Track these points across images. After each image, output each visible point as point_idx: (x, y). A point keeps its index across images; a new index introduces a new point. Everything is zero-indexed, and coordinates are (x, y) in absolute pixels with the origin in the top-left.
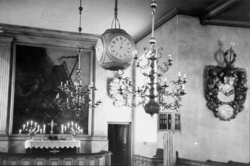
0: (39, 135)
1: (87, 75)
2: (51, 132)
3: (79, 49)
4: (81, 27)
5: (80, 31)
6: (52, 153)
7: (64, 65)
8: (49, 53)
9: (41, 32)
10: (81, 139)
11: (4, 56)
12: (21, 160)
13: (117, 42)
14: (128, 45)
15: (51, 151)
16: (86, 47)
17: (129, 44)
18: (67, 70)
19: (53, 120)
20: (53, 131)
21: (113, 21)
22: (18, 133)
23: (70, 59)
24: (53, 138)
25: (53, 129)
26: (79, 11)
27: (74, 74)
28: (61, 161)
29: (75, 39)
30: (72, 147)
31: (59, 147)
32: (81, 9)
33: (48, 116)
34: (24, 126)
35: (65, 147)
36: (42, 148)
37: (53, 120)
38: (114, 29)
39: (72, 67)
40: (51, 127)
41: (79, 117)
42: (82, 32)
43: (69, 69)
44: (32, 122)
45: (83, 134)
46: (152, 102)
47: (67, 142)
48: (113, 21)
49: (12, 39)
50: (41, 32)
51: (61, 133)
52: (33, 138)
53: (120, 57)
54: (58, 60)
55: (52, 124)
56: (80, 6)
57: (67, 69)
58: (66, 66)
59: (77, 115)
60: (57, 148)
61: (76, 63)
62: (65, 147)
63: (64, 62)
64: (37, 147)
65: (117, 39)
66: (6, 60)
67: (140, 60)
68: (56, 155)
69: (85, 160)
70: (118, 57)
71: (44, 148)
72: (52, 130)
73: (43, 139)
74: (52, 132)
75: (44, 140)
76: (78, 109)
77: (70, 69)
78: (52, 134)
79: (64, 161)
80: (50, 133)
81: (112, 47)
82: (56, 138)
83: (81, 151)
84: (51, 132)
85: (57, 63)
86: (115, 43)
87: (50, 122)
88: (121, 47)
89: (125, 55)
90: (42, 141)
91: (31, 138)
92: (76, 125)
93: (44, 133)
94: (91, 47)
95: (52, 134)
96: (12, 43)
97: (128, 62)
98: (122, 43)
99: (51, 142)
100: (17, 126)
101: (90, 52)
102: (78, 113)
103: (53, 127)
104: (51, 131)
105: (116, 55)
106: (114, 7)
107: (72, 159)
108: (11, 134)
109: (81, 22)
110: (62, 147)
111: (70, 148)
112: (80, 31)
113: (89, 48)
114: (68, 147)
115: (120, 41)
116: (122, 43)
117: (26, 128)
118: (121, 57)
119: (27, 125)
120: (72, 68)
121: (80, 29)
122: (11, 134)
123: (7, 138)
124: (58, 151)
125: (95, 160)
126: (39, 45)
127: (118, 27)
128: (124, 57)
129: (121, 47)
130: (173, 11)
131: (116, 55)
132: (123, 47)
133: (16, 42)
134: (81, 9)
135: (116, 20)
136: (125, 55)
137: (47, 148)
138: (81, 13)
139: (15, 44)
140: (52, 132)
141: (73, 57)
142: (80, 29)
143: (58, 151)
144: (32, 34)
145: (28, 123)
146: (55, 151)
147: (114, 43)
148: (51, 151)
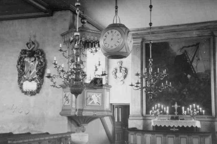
0: (201, 116)
1: (207, 60)
2: (175, 113)
3: (149, 42)
4: (152, 22)
5: (151, 25)
6: (172, 131)
7: (185, 53)
8: (172, 45)
9: (163, 30)
10: (200, 120)
12: (136, 135)
13: (108, 36)
14: (118, 36)
15: (171, 129)
16: (206, 35)
17: (118, 35)
18: (188, 58)
19: (176, 103)
20: (177, 112)
21: (114, 18)
22: (149, 114)
23: (190, 48)
24: (175, 118)
25: (177, 110)
26: (149, 9)
27: (195, 60)
28: (177, 138)
29: (194, 29)
30: (190, 126)
31: (178, 126)
32: (151, 7)
34: (153, 108)
35: (183, 126)
36: (163, 126)
37: (176, 103)
38: (115, 24)
39: (192, 55)
40: (175, 109)
41: (152, 99)
42: (153, 26)
43: (190, 57)
44: (159, 104)
45: (205, 115)
46: (77, 84)
47: (185, 122)
48: (114, 18)
49: (141, 39)
50: (163, 30)
51: (182, 114)
52: (157, 118)
53: (111, 47)
54: (179, 50)
55: (176, 106)
56: (150, 5)
57: (188, 56)
58: (187, 55)
59: (151, 98)
60: (176, 126)
61: (196, 51)
62: (183, 126)
63: (185, 51)
64: (159, 125)
65: (108, 33)
66: (136, 56)
67: (64, 52)
68: (173, 133)
69: (187, 138)
70: (109, 47)
71: (165, 126)
72: (176, 111)
74: (176, 113)
75: (168, 119)
76: (150, 92)
77: (191, 56)
78: (176, 114)
79: (167, 137)
80: (175, 114)
81: (105, 40)
82: (177, 118)
83: (203, 130)
84: (175, 113)
85: (179, 53)
86: (107, 37)
87: (174, 104)
88: (112, 39)
89: (116, 45)
90: (167, 120)
91: (156, 117)
92: (198, 106)
93: (168, 113)
94: (210, 33)
95: (176, 114)
96: (142, 42)
97: (120, 50)
98: (113, 35)
99: (171, 122)
100: (148, 109)
101: (210, 39)
102: (150, 96)
103: (177, 109)
104: (175, 112)
105: (108, 46)
106: (115, 5)
107: (186, 136)
108: (145, 115)
109: (151, 17)
110: (181, 126)
111: (188, 127)
112: (151, 25)
113: (210, 35)
114: (185, 126)
115: (111, 34)
118: (112, 47)
119: (156, 107)
120: (193, 56)
121: (151, 24)
122: (145, 114)
123: (141, 118)
124: (178, 130)
125: (199, 138)
126: (160, 41)
127: (118, 22)
128: (114, 47)
129: (112, 39)
130: (72, 7)
131: (108, 46)
132: (113, 39)
134: (151, 7)
135: (116, 17)
136: (116, 45)
137: (167, 126)
138: (151, 11)
139: (145, 43)
140: (176, 113)
141: (193, 45)
142: (151, 24)
143: (178, 130)
144: (156, 33)
145: (156, 106)
146: (174, 130)
147: (106, 37)
148: (171, 129)
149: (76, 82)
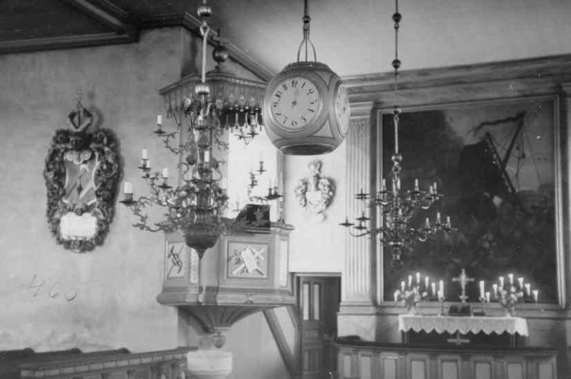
0: (530, 306)
1: (545, 159)
2: (461, 297)
4: (399, 58)
5: (396, 67)
6: (454, 343)
7: (488, 141)
8: (451, 119)
9: (428, 78)
10: (527, 315)
11: (358, 143)
12: (357, 354)
13: (285, 94)
14: (310, 95)
15: (450, 340)
16: (541, 91)
17: (312, 93)
18: (496, 152)
19: (463, 271)
20: (466, 295)
21: (300, 47)
22: (393, 300)
23: (501, 126)
24: (459, 310)
25: (466, 290)
26: (393, 23)
27: (512, 159)
28: (466, 363)
29: (510, 76)
30: (499, 332)
31: (468, 331)
32: (397, 17)
33: (457, 261)
34: (403, 284)
35: (482, 332)
36: (428, 331)
37: (463, 271)
38: (302, 62)
39: (505, 145)
40: (461, 286)
41: (399, 261)
42: (402, 68)
43: (499, 150)
44: (418, 275)
46: (202, 221)
47: (486, 321)
48: (300, 47)
49: (371, 103)
50: (428, 78)
51: (480, 299)
52: (413, 310)
53: (292, 124)
54: (472, 133)
55: (463, 279)
56: (395, 12)
57: (495, 148)
58: (492, 144)
59: (396, 257)
60: (463, 332)
61: (517, 134)
62: (482, 332)
63: (488, 134)
64: (417, 330)
65: (285, 87)
66: (358, 146)
67: (169, 136)
68: (455, 349)
69: (493, 363)
70: (288, 124)
71: (434, 332)
72: (464, 292)
73: (440, 312)
74: (463, 297)
75: (442, 314)
77: (503, 148)
78: (464, 301)
79: (439, 361)
80: (460, 301)
81: (275, 105)
82: (465, 312)
83: (534, 342)
84: (461, 297)
86: (282, 96)
87: (458, 274)
88: (294, 103)
89: (305, 119)
90: (439, 316)
91: (409, 309)
92: (521, 280)
93: (442, 298)
94: (553, 88)
95: (464, 301)
96: (374, 111)
97: (315, 132)
98: (297, 93)
99: (449, 320)
100: (389, 288)
101: (552, 102)
102: (396, 252)
103: (466, 286)
104: (461, 294)
105: (284, 122)
106: (303, 14)
107: (490, 358)
108: (381, 303)
109: (398, 45)
110: (475, 332)
111: (494, 334)
112: (396, 67)
114: (487, 332)
115: (291, 90)
116: (297, 93)
117: (407, 288)
118: (294, 124)
119: (410, 282)
120: (507, 147)
122: (383, 301)
123: (372, 310)
124: (467, 341)
125: (524, 363)
126: (421, 107)
127: (311, 59)
128: (301, 124)
129: (294, 103)
130: (191, 18)
131: (284, 122)
132: (297, 102)
133: (383, 108)
134: (397, 17)
135: (304, 44)
136: (305, 119)
137: (439, 331)
138: (396, 28)
139: (380, 113)
140: (463, 297)
141: (508, 120)
142: (396, 63)
143: (467, 341)
145: (410, 278)
146: (458, 341)
147: (279, 96)
148: (450, 340)
149: (200, 215)
